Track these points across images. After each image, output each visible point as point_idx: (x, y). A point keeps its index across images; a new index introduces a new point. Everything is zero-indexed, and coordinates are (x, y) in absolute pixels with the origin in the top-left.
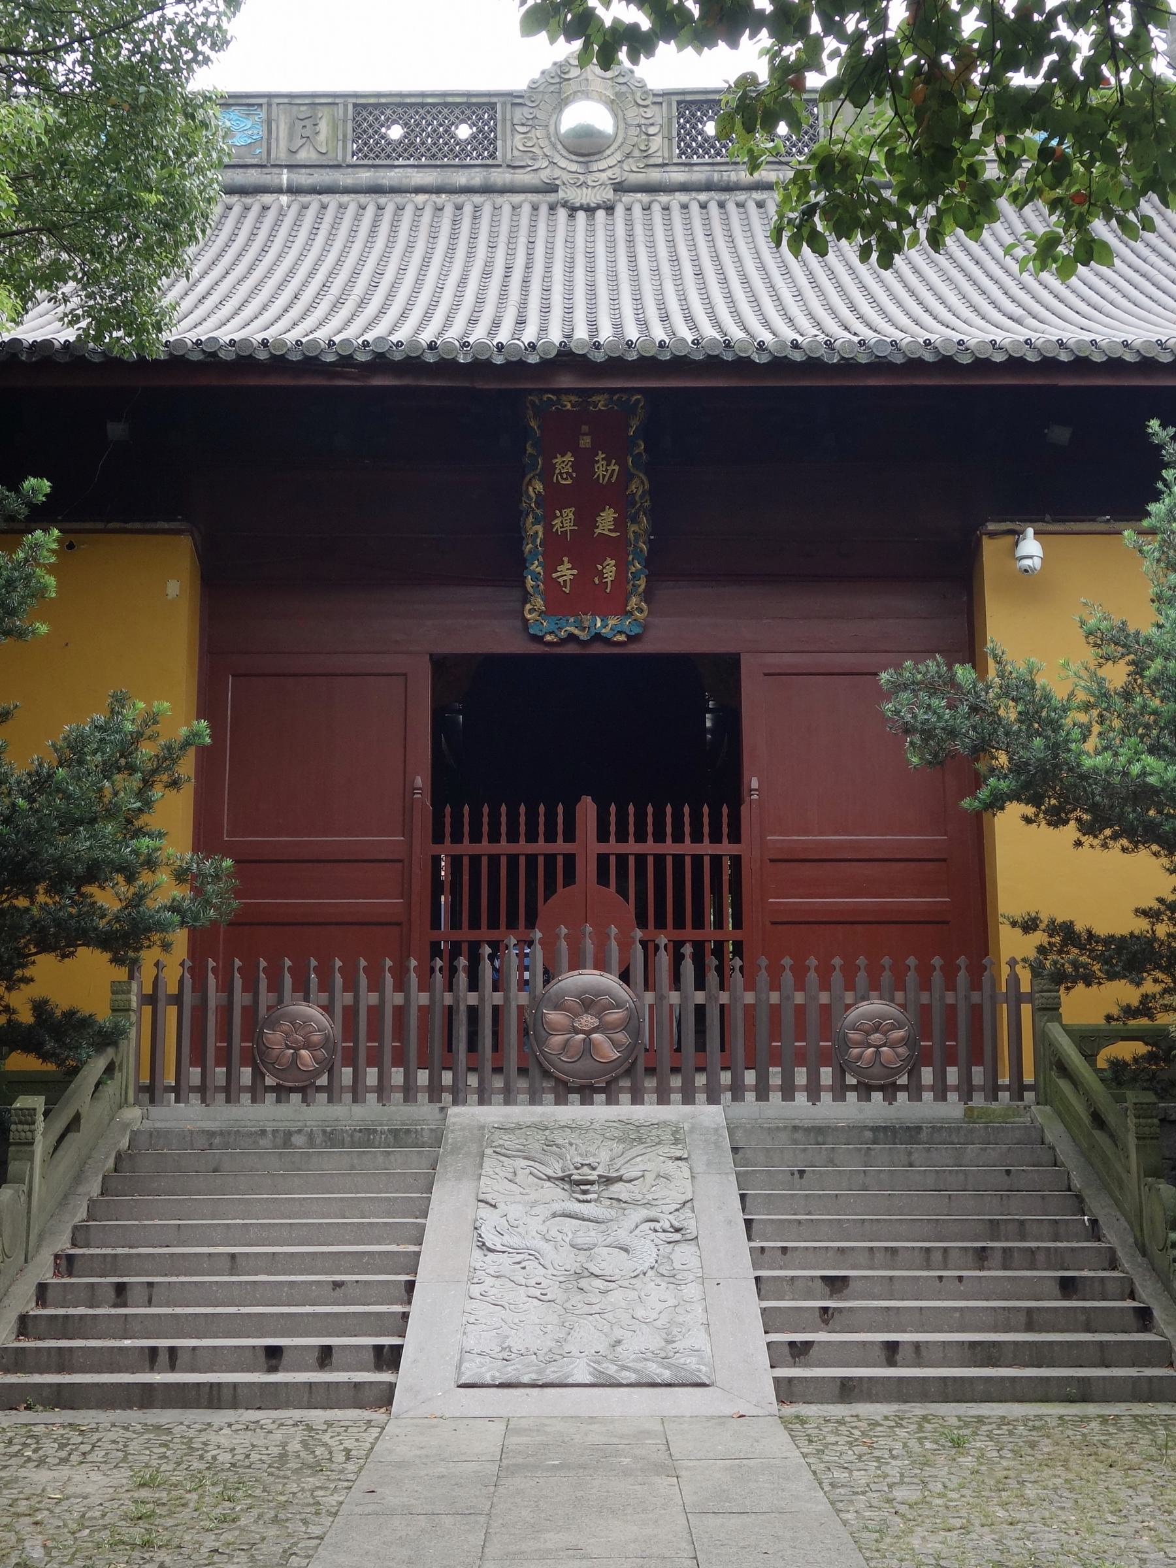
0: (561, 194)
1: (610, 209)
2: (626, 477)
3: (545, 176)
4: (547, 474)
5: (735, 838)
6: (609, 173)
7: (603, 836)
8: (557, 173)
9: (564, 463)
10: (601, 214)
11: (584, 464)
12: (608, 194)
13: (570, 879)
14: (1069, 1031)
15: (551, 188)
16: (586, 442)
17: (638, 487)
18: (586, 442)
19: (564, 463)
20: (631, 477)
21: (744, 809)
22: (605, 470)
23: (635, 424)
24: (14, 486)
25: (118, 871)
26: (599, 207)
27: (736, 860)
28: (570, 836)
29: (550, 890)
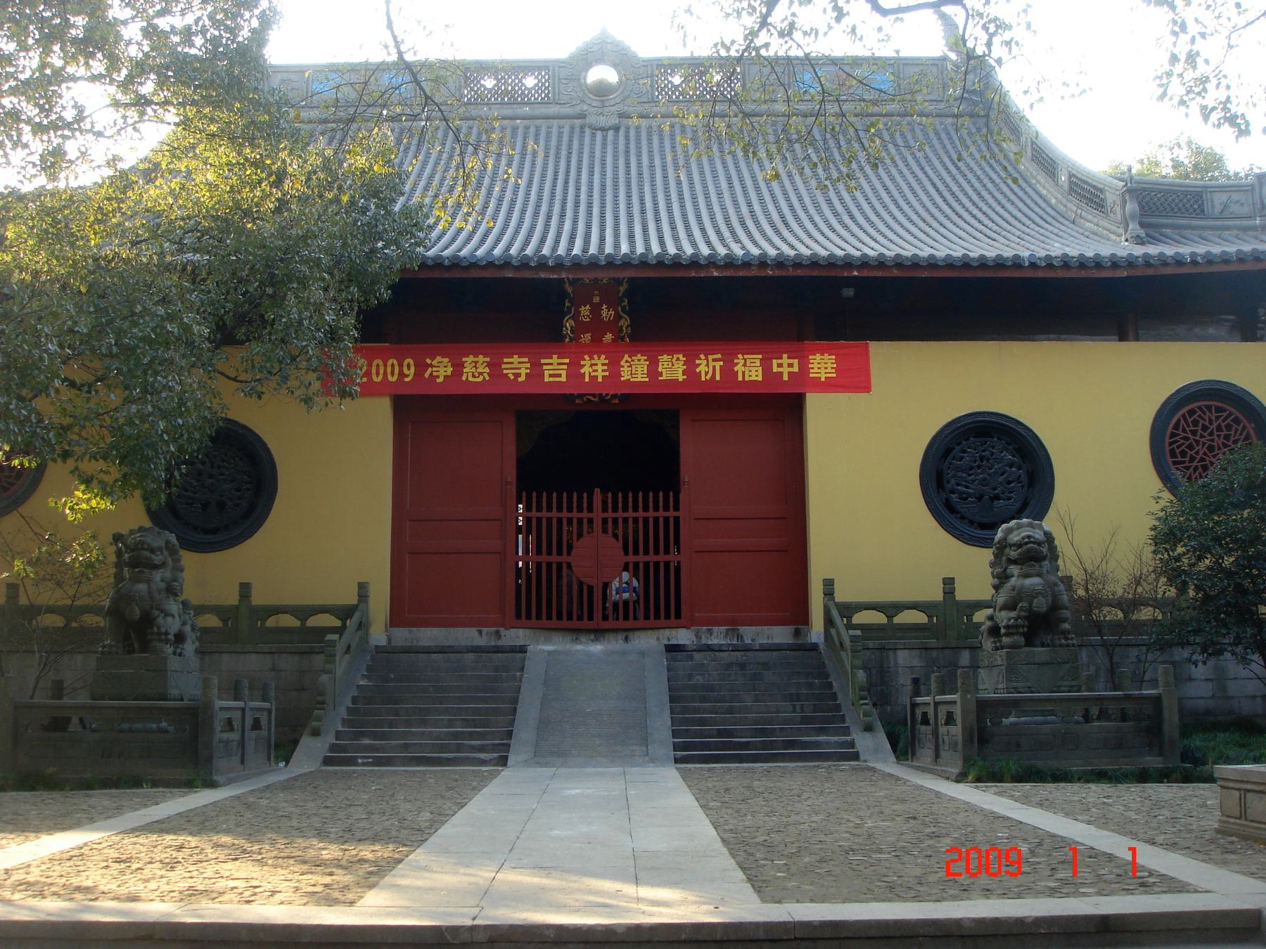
0: (587, 121)
1: (616, 129)
2: (618, 317)
3: (578, 109)
4: (576, 317)
5: (677, 508)
6: (616, 108)
7: (605, 510)
8: (585, 108)
9: (585, 310)
10: (611, 133)
11: (596, 311)
12: (614, 121)
13: (591, 531)
14: (837, 604)
15: (582, 116)
16: (596, 300)
17: (625, 322)
18: (596, 300)
19: (585, 310)
20: (621, 318)
21: (681, 495)
22: (606, 313)
23: (622, 289)
24: (5, 8)
25: (39, 466)
26: (610, 128)
27: (677, 519)
28: (590, 510)
29: (580, 535)
